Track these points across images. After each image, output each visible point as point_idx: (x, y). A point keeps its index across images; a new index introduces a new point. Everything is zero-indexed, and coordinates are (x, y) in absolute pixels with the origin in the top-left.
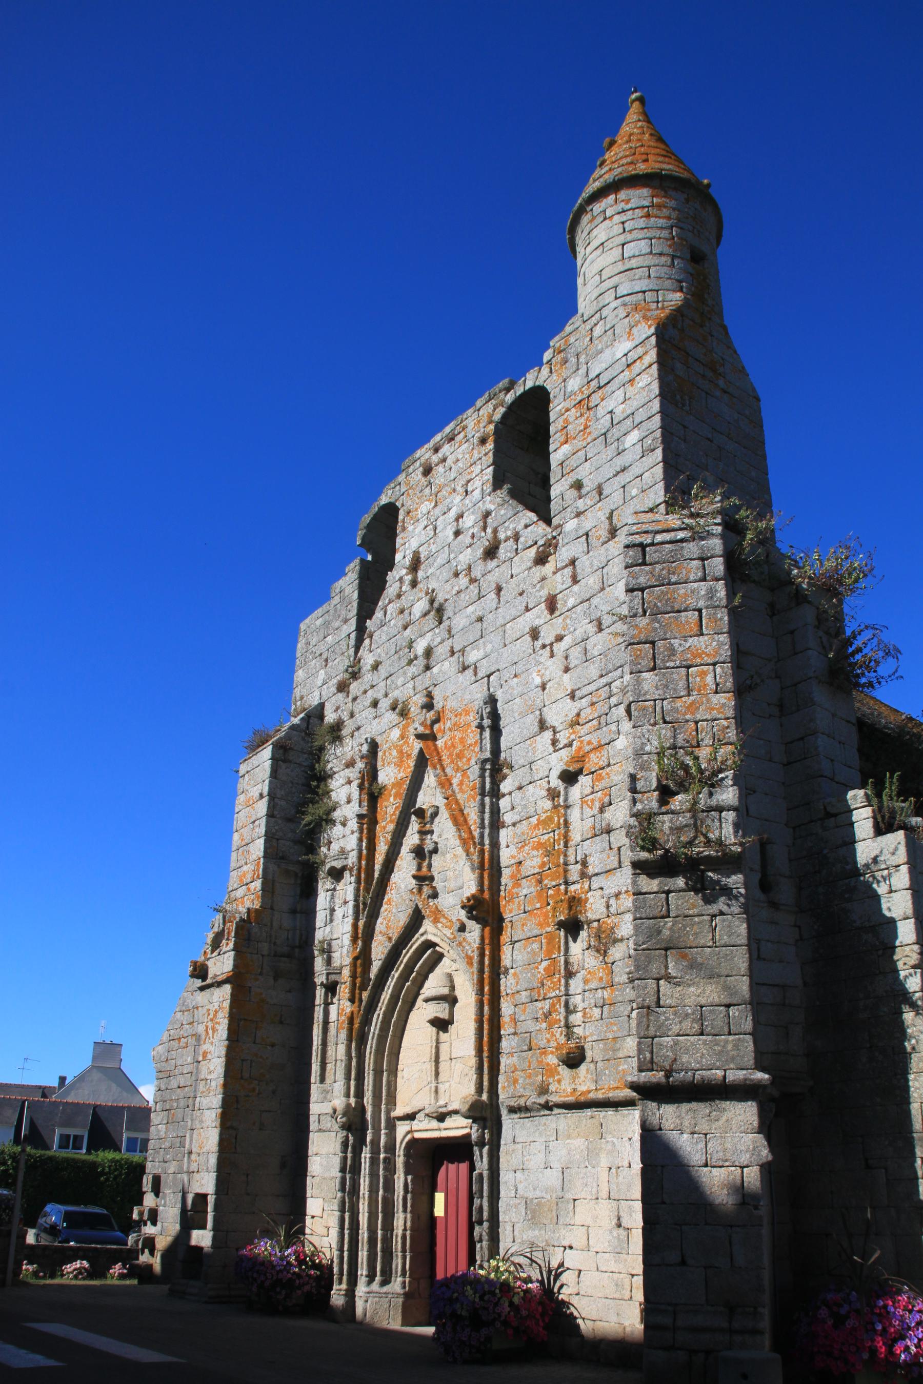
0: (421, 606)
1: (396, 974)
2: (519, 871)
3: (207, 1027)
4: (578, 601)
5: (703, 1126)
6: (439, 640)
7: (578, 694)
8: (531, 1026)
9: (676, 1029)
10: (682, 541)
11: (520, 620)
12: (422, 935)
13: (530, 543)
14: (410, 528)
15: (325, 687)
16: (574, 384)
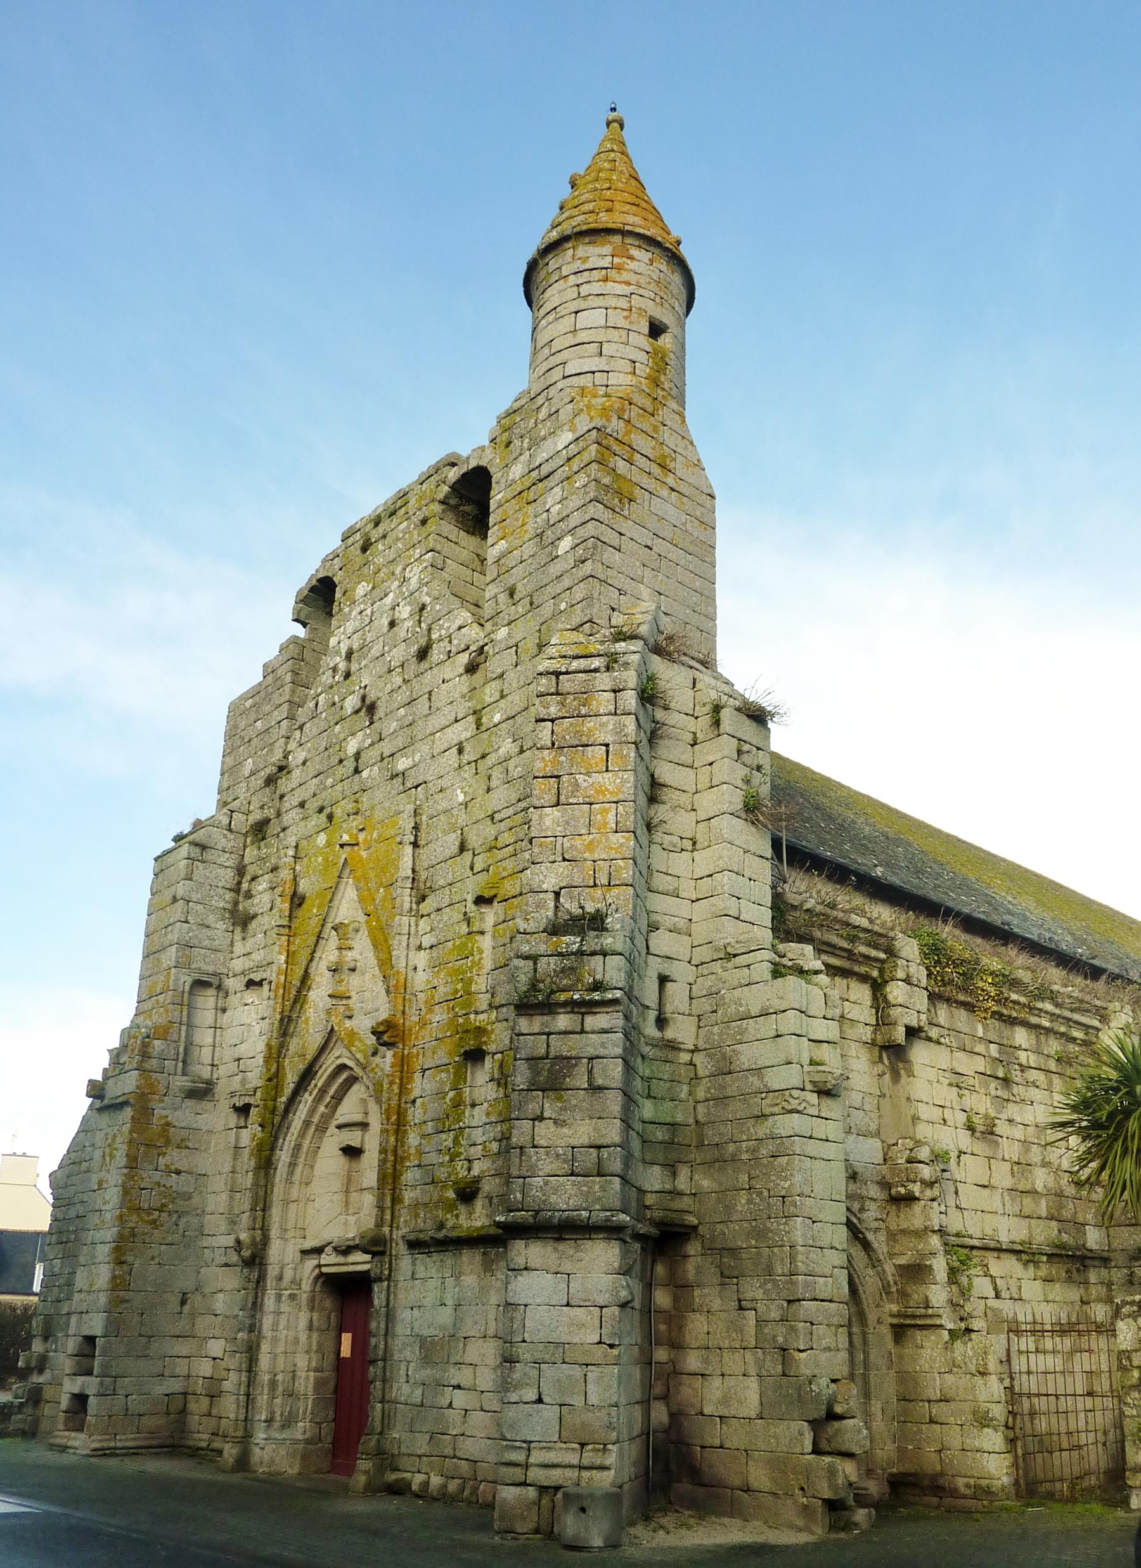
0: (352, 702)
2: (433, 997)
3: (104, 1153)
4: (504, 717)
5: (567, 1266)
6: (369, 741)
7: (497, 817)
8: (434, 1158)
9: (547, 1169)
10: (596, 670)
11: (449, 730)
12: (337, 1058)
13: (463, 647)
14: (347, 610)
15: (253, 778)
16: (517, 471)
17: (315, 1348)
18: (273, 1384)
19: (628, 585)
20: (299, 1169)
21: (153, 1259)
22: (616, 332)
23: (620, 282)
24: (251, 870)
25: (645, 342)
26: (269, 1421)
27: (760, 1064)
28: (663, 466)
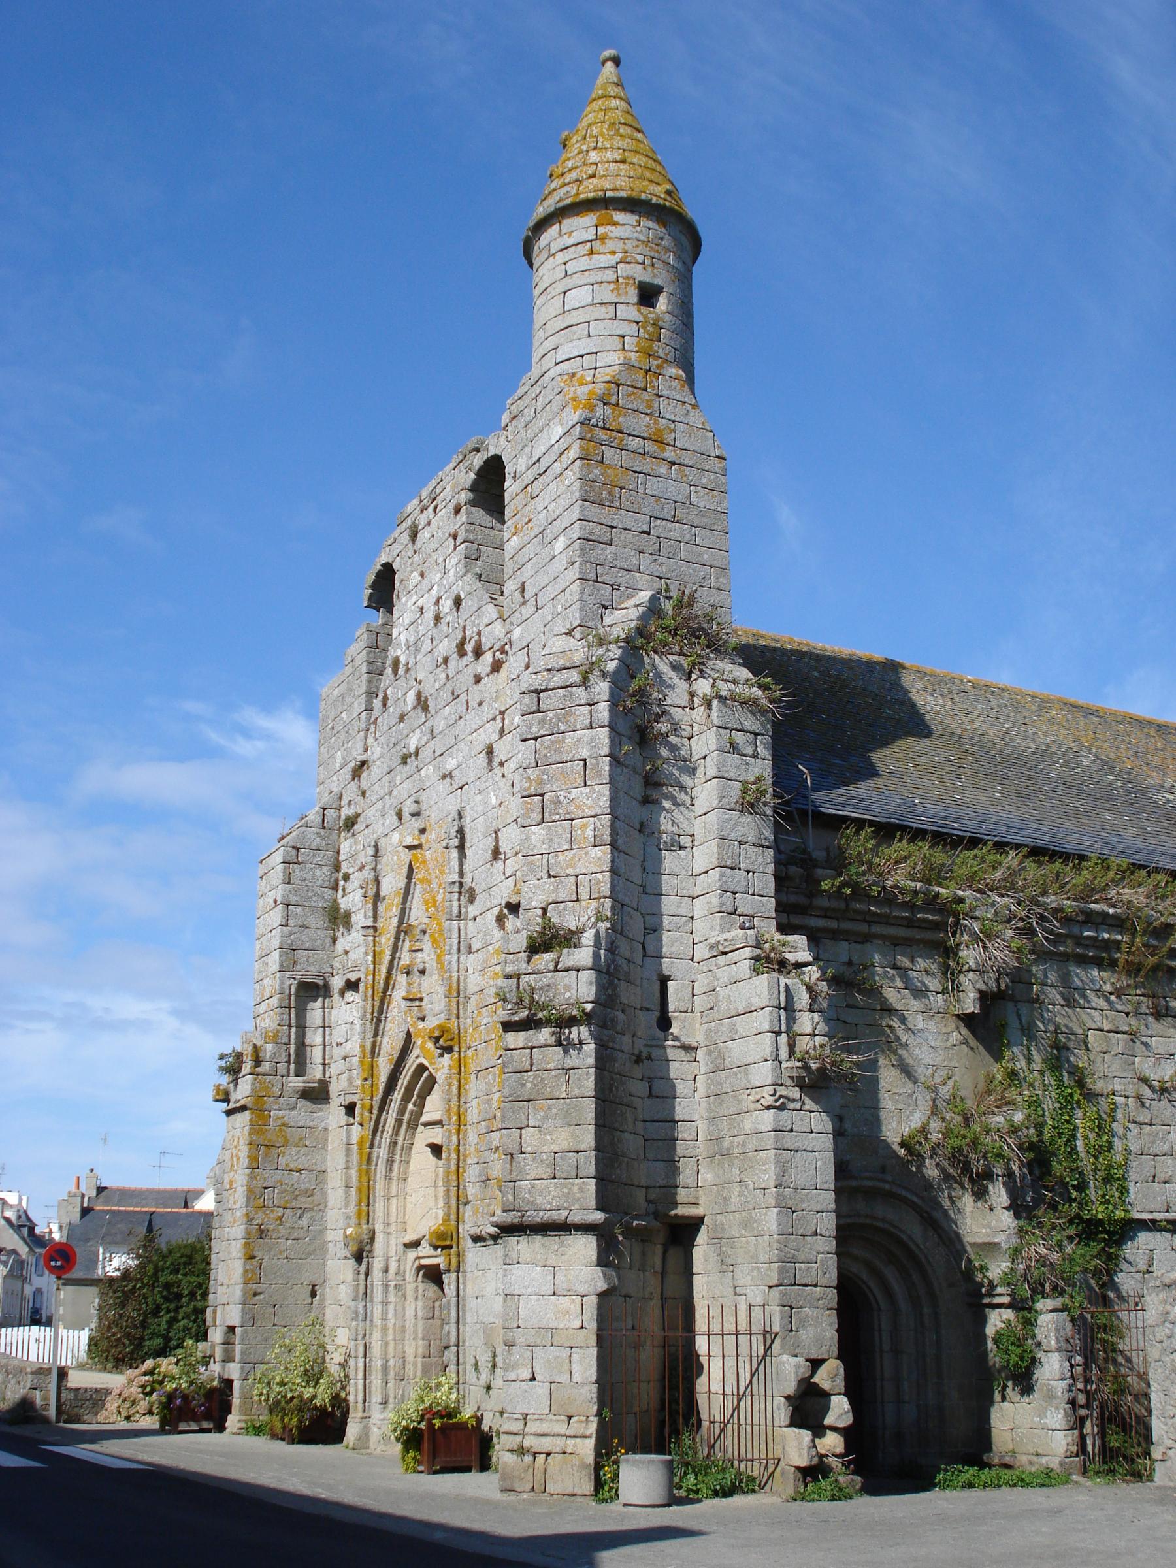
1: (397, 1096)
5: (552, 1261)
6: (425, 739)
9: (533, 1174)
17: (420, 1336)
18: (385, 1368)
19: (623, 579)
20: (396, 1166)
21: (281, 1253)
22: (603, 309)
23: (604, 254)
24: (344, 867)
25: (633, 313)
26: (385, 1403)
27: (745, 1061)
28: (659, 441)
